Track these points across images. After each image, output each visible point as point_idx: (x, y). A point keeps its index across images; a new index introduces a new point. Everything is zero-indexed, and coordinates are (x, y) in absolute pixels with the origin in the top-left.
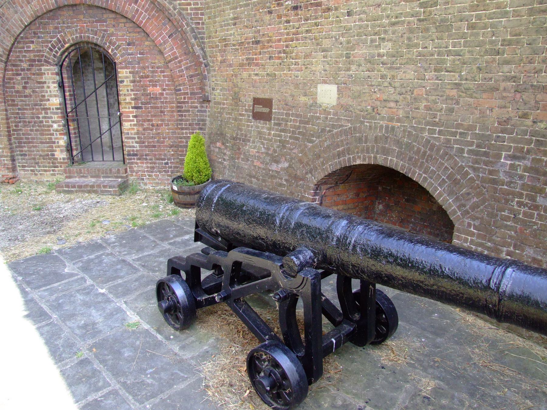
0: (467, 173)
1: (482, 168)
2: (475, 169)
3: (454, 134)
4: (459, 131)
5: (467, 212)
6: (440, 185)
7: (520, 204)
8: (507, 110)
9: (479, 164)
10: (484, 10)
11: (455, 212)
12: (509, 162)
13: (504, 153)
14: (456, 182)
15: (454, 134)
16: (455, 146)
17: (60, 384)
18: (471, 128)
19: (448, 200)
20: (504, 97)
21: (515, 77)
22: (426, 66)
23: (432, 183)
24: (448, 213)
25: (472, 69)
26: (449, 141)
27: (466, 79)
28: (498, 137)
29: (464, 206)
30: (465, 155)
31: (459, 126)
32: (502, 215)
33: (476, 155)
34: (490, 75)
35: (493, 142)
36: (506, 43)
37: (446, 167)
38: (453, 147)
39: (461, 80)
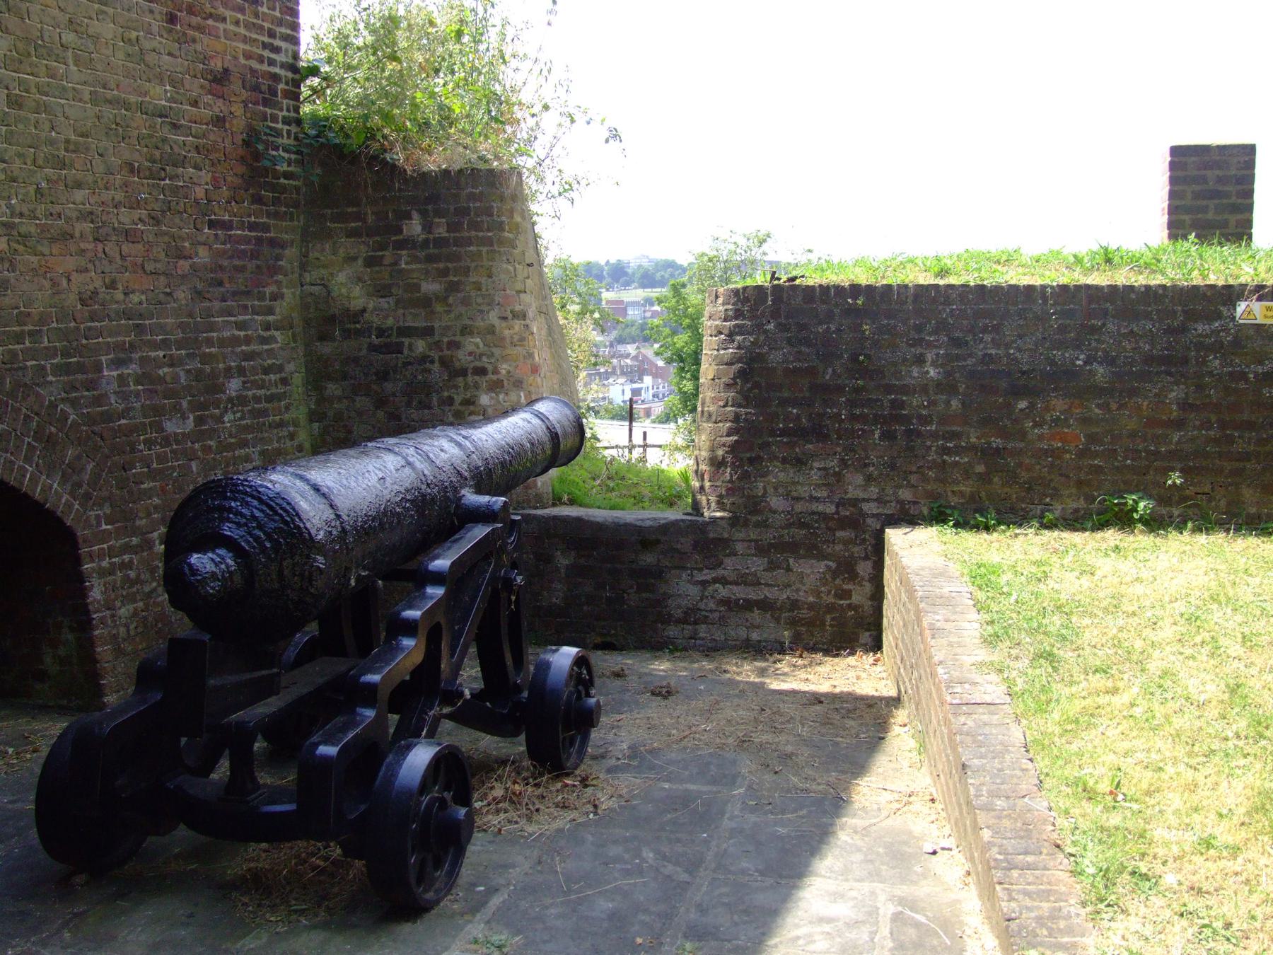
0: (65, 416)
1: (82, 397)
2: (74, 403)
3: (19, 338)
4: (26, 328)
5: (88, 496)
6: (28, 459)
7: (149, 443)
8: (88, 275)
9: (76, 389)
10: (32, 74)
11: (69, 506)
12: (115, 373)
13: (103, 358)
14: (50, 442)
15: (19, 338)
16: (29, 363)
17: (592, 259)
18: (43, 320)
19: (51, 488)
20: (83, 251)
21: (91, 213)
22: (1148, 931)
23: (11, 462)
24: (59, 514)
25: (27, 193)
26: (14, 354)
27: (21, 215)
28: (90, 329)
29: (79, 485)
30: (50, 378)
31: (22, 319)
32: (134, 475)
33: (67, 374)
34: (58, 208)
35: (84, 341)
36: (72, 147)
37: (27, 416)
38: (26, 368)
39: (12, 216)
